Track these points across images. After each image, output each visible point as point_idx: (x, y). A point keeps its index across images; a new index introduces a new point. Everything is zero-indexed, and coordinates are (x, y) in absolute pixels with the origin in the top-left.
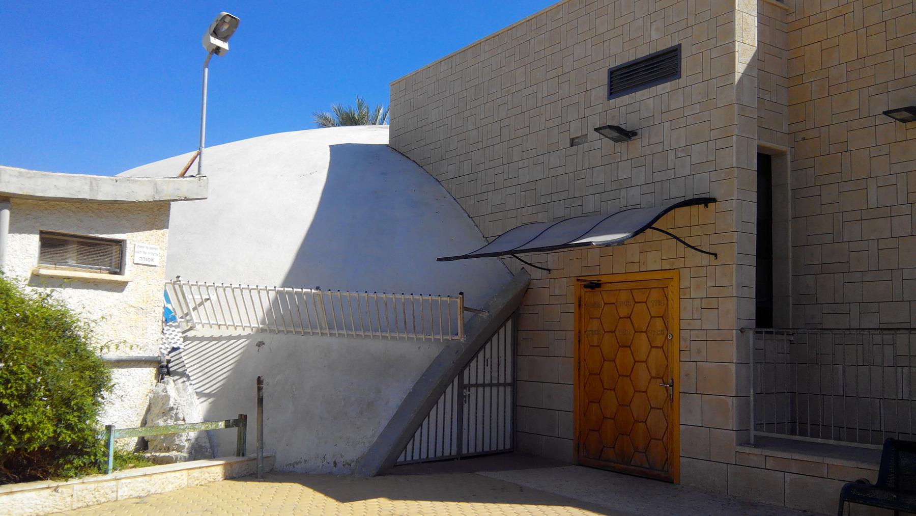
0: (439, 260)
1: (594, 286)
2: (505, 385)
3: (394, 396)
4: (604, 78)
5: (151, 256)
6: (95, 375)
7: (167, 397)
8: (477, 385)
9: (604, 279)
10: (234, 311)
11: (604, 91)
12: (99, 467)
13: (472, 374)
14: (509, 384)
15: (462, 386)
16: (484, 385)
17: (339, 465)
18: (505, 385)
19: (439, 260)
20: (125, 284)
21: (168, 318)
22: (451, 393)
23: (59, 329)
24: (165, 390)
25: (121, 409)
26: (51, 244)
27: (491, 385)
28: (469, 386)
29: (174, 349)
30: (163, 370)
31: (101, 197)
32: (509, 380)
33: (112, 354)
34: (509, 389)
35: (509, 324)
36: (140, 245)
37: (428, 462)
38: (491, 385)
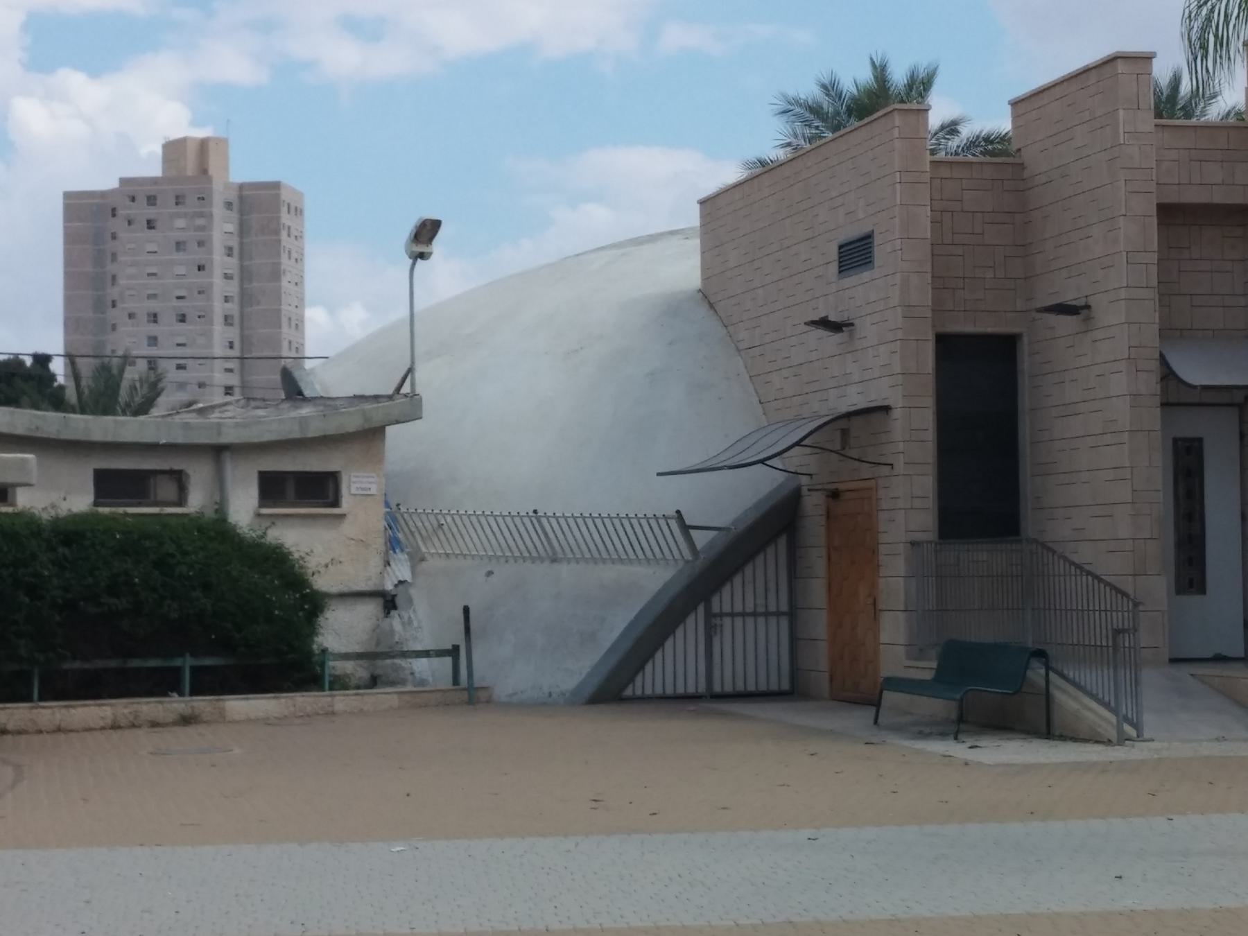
0: (659, 474)
1: (835, 495)
2: (778, 614)
3: (617, 624)
4: (833, 253)
5: (368, 486)
6: (313, 605)
7: (392, 632)
8: (732, 615)
9: (841, 487)
10: (467, 537)
11: (834, 267)
12: (321, 688)
13: (724, 600)
14: (784, 614)
15: (709, 615)
16: (743, 614)
17: (554, 695)
18: (778, 614)
19: (659, 474)
20: (343, 516)
21: (393, 544)
22: (694, 625)
23: (279, 566)
24: (391, 625)
25: (341, 631)
26: (273, 488)
27: (754, 614)
28: (721, 615)
29: (401, 582)
30: (389, 603)
31: (310, 435)
32: (784, 607)
33: (688, 555)
34: (785, 622)
35: (782, 542)
36: (358, 485)
37: (664, 698)
38: (754, 614)
